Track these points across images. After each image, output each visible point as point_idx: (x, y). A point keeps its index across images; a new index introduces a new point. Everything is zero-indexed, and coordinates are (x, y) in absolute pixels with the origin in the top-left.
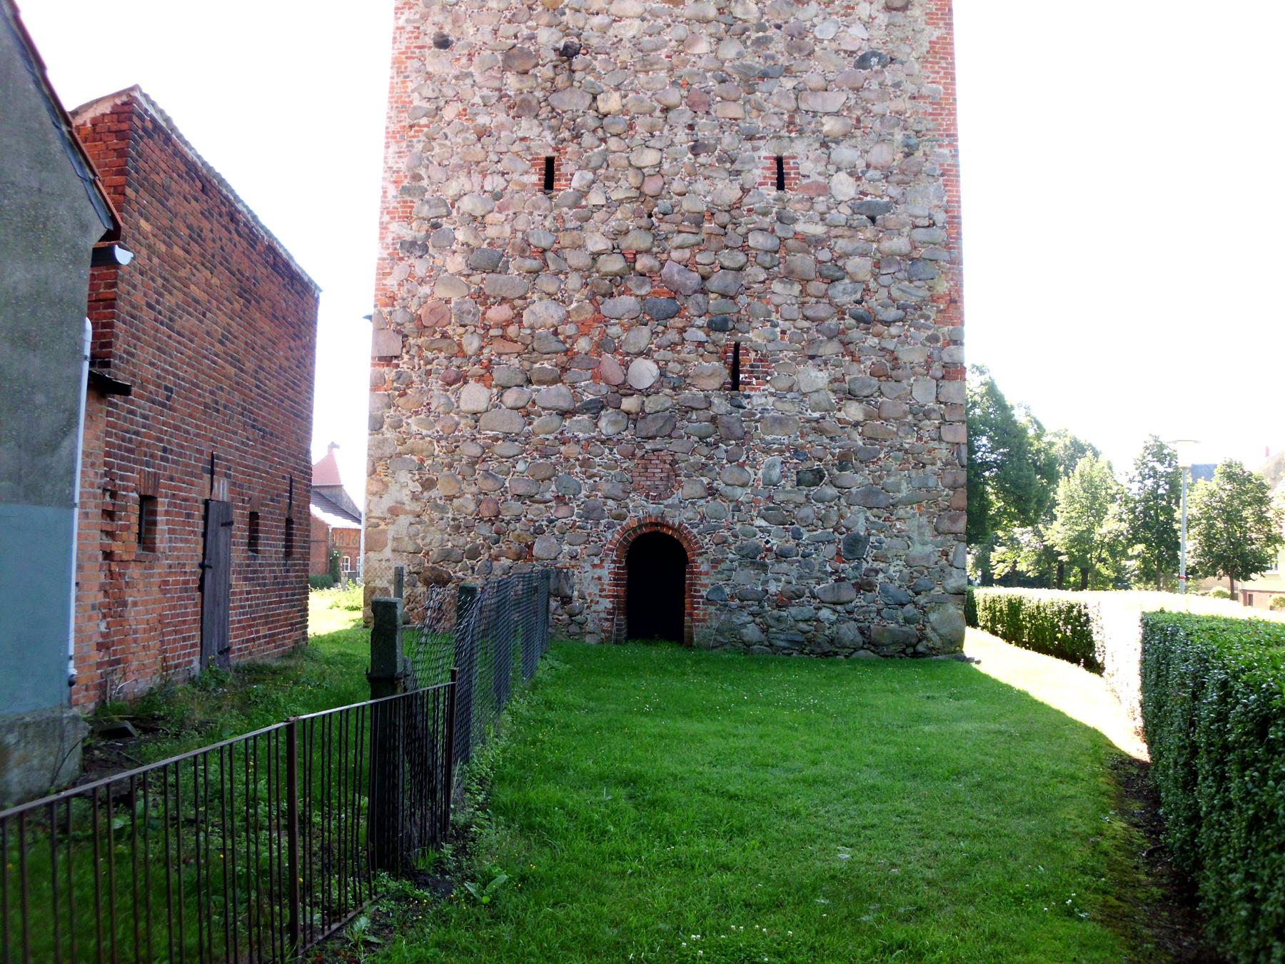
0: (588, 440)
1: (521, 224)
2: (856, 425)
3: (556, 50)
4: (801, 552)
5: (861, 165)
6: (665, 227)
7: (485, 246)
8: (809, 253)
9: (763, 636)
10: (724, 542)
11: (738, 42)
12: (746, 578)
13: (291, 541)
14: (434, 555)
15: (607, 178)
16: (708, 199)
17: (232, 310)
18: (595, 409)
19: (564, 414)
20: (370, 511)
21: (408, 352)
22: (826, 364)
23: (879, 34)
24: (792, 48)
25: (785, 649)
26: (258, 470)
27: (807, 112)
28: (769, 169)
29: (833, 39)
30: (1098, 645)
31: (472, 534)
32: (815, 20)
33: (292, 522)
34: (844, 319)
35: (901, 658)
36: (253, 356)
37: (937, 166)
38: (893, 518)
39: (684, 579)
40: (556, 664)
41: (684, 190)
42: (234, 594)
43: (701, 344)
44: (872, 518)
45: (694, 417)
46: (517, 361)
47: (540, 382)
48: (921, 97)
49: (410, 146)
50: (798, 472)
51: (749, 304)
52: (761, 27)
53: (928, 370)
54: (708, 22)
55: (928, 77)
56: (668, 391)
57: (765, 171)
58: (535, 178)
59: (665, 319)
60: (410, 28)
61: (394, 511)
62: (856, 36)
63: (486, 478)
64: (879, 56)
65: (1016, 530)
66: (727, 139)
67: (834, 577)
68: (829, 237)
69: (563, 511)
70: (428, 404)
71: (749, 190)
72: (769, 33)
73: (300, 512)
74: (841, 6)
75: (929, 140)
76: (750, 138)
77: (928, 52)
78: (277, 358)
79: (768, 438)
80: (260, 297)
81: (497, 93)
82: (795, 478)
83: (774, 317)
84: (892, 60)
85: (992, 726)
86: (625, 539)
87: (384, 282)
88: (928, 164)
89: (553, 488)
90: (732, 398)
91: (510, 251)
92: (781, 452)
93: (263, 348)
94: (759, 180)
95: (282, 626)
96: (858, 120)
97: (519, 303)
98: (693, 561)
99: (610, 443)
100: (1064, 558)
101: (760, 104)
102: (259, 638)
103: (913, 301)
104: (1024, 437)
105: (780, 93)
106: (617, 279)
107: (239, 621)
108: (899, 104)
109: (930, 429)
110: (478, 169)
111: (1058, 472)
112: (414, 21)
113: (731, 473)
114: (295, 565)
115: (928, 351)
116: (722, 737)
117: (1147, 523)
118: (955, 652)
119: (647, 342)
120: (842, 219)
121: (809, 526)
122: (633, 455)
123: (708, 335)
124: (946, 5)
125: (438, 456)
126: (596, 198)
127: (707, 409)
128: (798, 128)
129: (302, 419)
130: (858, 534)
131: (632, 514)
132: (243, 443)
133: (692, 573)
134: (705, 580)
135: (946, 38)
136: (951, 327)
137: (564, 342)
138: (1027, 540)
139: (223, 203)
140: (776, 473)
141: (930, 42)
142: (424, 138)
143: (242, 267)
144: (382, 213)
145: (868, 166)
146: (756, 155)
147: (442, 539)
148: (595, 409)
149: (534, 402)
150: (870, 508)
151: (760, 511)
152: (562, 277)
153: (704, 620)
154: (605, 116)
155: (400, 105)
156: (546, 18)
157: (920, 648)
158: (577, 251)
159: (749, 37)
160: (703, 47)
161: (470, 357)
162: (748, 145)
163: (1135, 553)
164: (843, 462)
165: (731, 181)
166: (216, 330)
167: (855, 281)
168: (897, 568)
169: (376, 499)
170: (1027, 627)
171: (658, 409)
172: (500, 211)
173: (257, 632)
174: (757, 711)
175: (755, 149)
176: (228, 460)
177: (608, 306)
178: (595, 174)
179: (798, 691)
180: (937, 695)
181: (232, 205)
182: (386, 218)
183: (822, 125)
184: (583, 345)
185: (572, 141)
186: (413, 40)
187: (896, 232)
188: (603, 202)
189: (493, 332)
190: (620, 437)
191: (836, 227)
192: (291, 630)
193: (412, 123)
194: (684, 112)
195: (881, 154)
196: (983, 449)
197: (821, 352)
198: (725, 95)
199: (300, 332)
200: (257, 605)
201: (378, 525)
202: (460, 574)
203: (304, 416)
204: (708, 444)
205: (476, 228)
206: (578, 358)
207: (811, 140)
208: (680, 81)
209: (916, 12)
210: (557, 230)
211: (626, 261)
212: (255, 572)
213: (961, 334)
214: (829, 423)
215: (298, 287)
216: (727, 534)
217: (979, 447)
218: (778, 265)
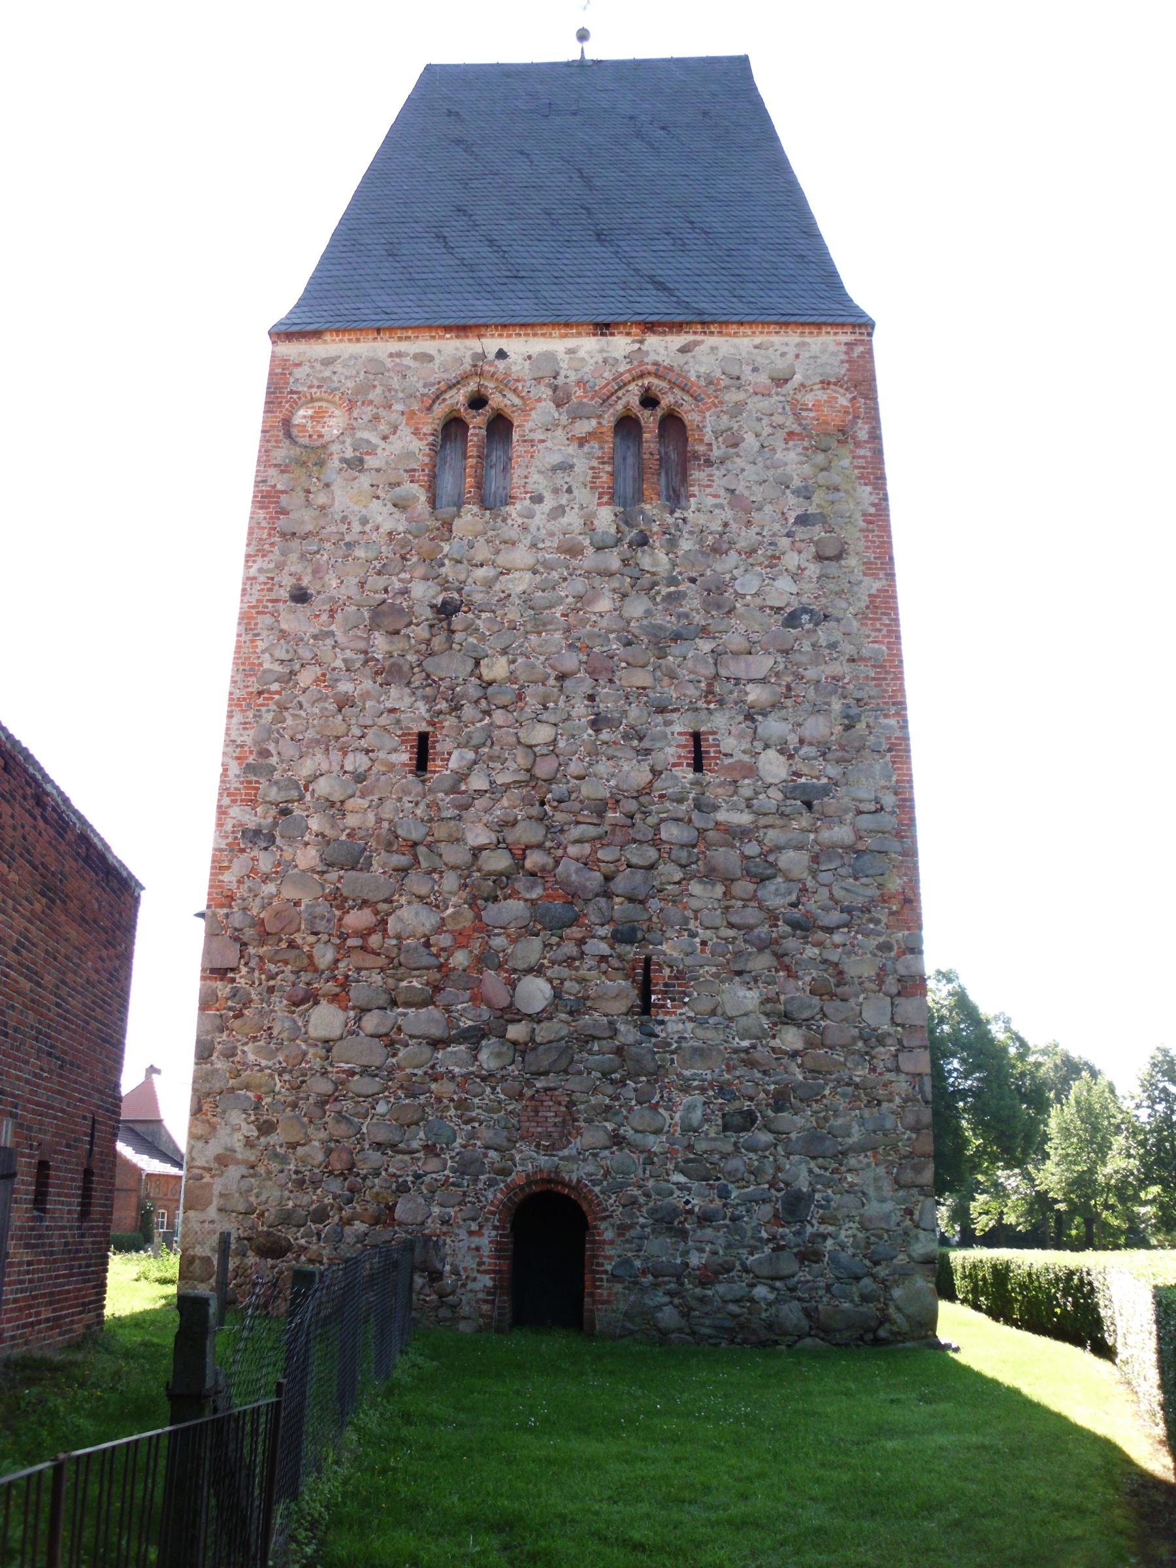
0: (466, 1076)
1: (387, 811)
2: (794, 1054)
3: (432, 606)
4: (729, 1214)
5: (793, 740)
6: (560, 817)
7: (343, 837)
8: (733, 847)
9: (683, 1322)
10: (633, 1203)
11: (646, 598)
12: (660, 1248)
13: (90, 1197)
14: (270, 1216)
15: (491, 758)
16: (612, 783)
17: (32, 911)
18: (474, 1037)
19: (436, 1043)
20: (193, 1159)
21: (246, 964)
22: (756, 981)
23: (809, 587)
24: (709, 605)
25: (710, 1337)
26: (53, 1108)
27: (728, 679)
28: (684, 746)
29: (757, 594)
30: (1107, 1322)
31: (319, 1191)
32: (735, 572)
33: (92, 1174)
34: (776, 926)
35: (858, 1346)
36: (54, 968)
37: (883, 740)
38: (843, 1169)
39: (583, 1250)
40: (420, 1360)
41: (582, 772)
42: (11, 1265)
43: (603, 958)
44: (817, 1171)
45: (596, 1048)
46: (379, 978)
47: (408, 1005)
48: (862, 659)
49: (258, 716)
50: (724, 1116)
51: (661, 910)
52: (672, 581)
53: (880, 985)
54: (611, 575)
55: (868, 636)
56: (563, 1016)
57: (680, 750)
58: (404, 757)
59: (560, 928)
60: (262, 579)
61: (223, 1160)
62: (783, 590)
63: (338, 1122)
64: (811, 612)
65: (999, 1173)
66: (635, 712)
67: (771, 1245)
68: (757, 827)
69: (433, 1164)
70: (269, 1028)
71: (661, 773)
72: (681, 588)
73: (103, 1161)
74: (764, 555)
75: (872, 710)
76: (662, 710)
77: (867, 607)
78: (84, 970)
79: (687, 1073)
80: (67, 896)
81: (362, 656)
82: (720, 1122)
83: (692, 925)
84: (826, 616)
85: (975, 1439)
86: (510, 1199)
87: (221, 877)
88: (872, 737)
89: (422, 1135)
90: (642, 1024)
91: (374, 844)
92: (703, 1090)
93: (67, 957)
94: (672, 760)
95: (70, 1307)
96: (789, 688)
97: (383, 907)
98: (595, 1227)
99: (493, 1079)
100: (1062, 1207)
101: (672, 671)
102: (39, 1322)
103: (859, 902)
104: (1003, 1058)
105: (695, 657)
106: (502, 879)
107: (15, 1301)
108: (835, 669)
109: (886, 1057)
110: (338, 745)
111: (1048, 1098)
112: (268, 571)
113: (642, 1116)
114: (92, 1228)
115: (879, 962)
116: (626, 1462)
117: (1162, 1158)
118: (926, 1337)
119: (538, 956)
120: (772, 805)
121: (739, 1181)
122: (521, 1095)
123: (612, 948)
124: (886, 553)
125: (279, 1093)
126: (477, 782)
127: (611, 1038)
128: (718, 698)
129: (113, 1045)
130: (800, 1190)
131: (520, 1168)
132: (35, 1075)
133: (594, 1242)
134: (609, 1251)
135: (887, 591)
136: (906, 933)
137: (437, 956)
138: (1014, 1184)
139: (28, 784)
140: (697, 1115)
141: (870, 596)
142: (275, 707)
143: (47, 860)
144: (221, 794)
145: (802, 741)
146: (668, 730)
147: (282, 1197)
148: (474, 1037)
149: (400, 1029)
150: (814, 1158)
151: (677, 1163)
152: (436, 876)
153: (608, 1302)
154: (490, 684)
155: (247, 668)
156: (421, 571)
157: (882, 1333)
158: (455, 846)
159: (658, 593)
160: (604, 604)
161: (323, 972)
162: (659, 719)
163: (1150, 1197)
164: (780, 1102)
165: (639, 762)
166: (11, 936)
167: (789, 880)
168: (849, 1232)
169: (200, 1144)
170: (1017, 1300)
171: (552, 1038)
172: (363, 796)
173: (38, 1314)
174: (671, 1425)
175: (667, 723)
176: (14, 1096)
177: (492, 913)
178: (476, 753)
179: (726, 1396)
180: (903, 1397)
181: (39, 785)
182: (226, 801)
183: (747, 694)
184: (460, 959)
185: (450, 714)
186: (265, 592)
187: (836, 819)
188: (486, 787)
189: (351, 942)
190: (504, 1072)
191: (765, 814)
192: (80, 1313)
193: (261, 688)
194: (582, 680)
195: (816, 727)
196: (955, 1074)
197: (750, 966)
198: (631, 660)
199: (114, 938)
200: (40, 1280)
201: (201, 1177)
202: (303, 1242)
203: (114, 1041)
204: (612, 1082)
205: (333, 816)
206: (454, 976)
207: (734, 711)
208: (578, 644)
209: (852, 561)
210: (431, 820)
211: (514, 858)
212: (40, 1237)
213: (919, 940)
214: (761, 1054)
215: (115, 885)
216: (636, 1192)
217: (950, 1072)
218: (696, 863)
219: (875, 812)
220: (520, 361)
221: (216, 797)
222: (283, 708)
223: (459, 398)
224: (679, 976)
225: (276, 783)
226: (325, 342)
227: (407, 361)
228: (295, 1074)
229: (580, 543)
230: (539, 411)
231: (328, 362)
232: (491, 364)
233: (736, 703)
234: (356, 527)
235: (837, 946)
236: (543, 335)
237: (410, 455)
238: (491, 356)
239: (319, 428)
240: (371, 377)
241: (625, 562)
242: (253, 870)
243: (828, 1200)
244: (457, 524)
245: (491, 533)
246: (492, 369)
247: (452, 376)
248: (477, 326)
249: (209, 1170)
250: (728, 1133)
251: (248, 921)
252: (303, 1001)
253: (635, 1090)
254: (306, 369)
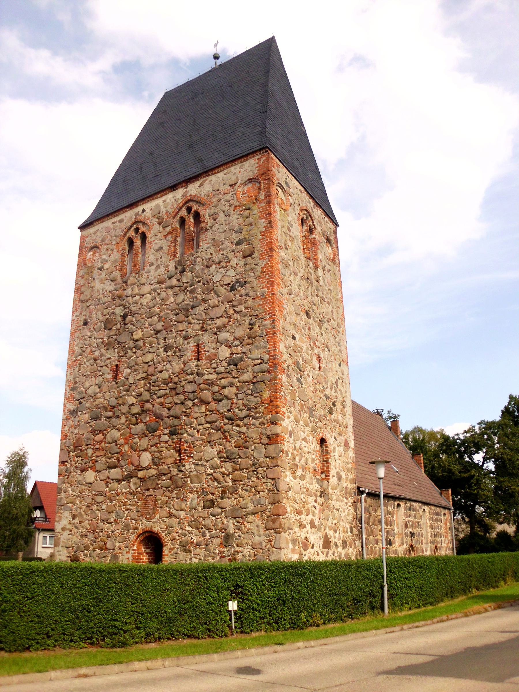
3: (121, 316)
62: (231, 276)
131: (141, 527)
175: (188, 343)
182: (66, 401)
219: (261, 363)
221: (63, 401)
238: (140, 212)
250: (205, 509)
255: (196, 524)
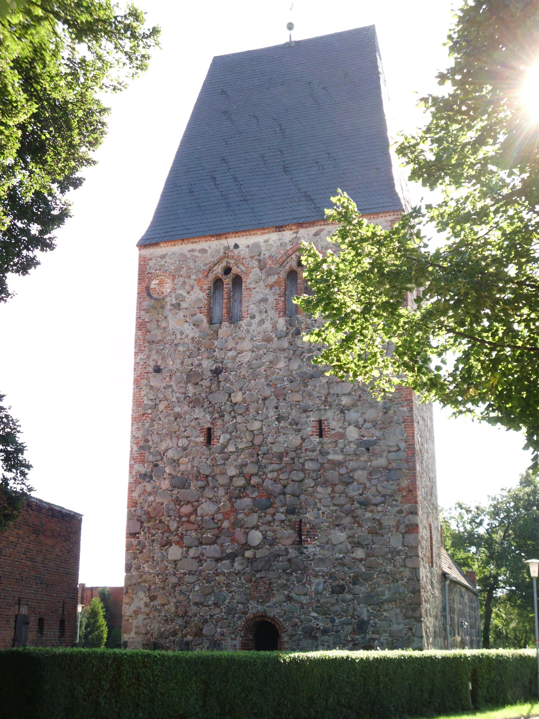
0: (229, 573)
1: (196, 463)
2: (361, 560)
3: (211, 371)
5: (361, 420)
6: (264, 461)
7: (179, 475)
8: (335, 470)
18: (232, 557)
19: (218, 560)
28: (315, 427)
37: (401, 418)
41: (273, 441)
43: (282, 521)
45: (281, 559)
47: (206, 544)
49: (143, 425)
54: (284, 350)
56: (267, 546)
60: (142, 363)
69: (217, 610)
75: (396, 404)
76: (305, 411)
79: (317, 569)
82: (330, 590)
83: (318, 505)
89: (213, 598)
92: (323, 576)
94: (310, 433)
96: (360, 396)
101: (310, 393)
103: (389, 492)
112: (144, 359)
115: (397, 518)
121: (340, 616)
123: (286, 516)
126: (231, 448)
131: (251, 611)
133: (280, 642)
137: (217, 523)
145: (365, 421)
146: (308, 420)
148: (232, 557)
149: (203, 555)
150: (369, 605)
154: (236, 404)
156: (206, 355)
160: (281, 364)
162: (304, 415)
172: (186, 457)
175: (308, 417)
182: (133, 462)
184: (226, 524)
188: (234, 450)
189: (184, 519)
195: (371, 414)
197: (342, 522)
201: (128, 620)
204: (287, 574)
205: (175, 466)
206: (224, 531)
210: (213, 466)
214: (347, 560)
216: (297, 620)
219: (397, 451)
220: (244, 249)
222: (153, 420)
223: (219, 270)
224: (313, 528)
225: (152, 453)
226: (161, 247)
227: (196, 254)
228: (163, 575)
229: (271, 336)
230: (253, 273)
231: (163, 257)
232: (232, 251)
233: (337, 406)
234: (179, 337)
235: (380, 512)
236: (254, 234)
237: (199, 300)
239: (161, 289)
240: (181, 263)
241: (291, 344)
242: (144, 491)
243: (376, 623)
244: (220, 331)
245: (234, 335)
246: (232, 254)
247: (215, 259)
248: (225, 234)
249: (131, 617)
251: (143, 513)
252: (165, 545)
253: (296, 577)
254: (154, 261)
255: (322, 610)
